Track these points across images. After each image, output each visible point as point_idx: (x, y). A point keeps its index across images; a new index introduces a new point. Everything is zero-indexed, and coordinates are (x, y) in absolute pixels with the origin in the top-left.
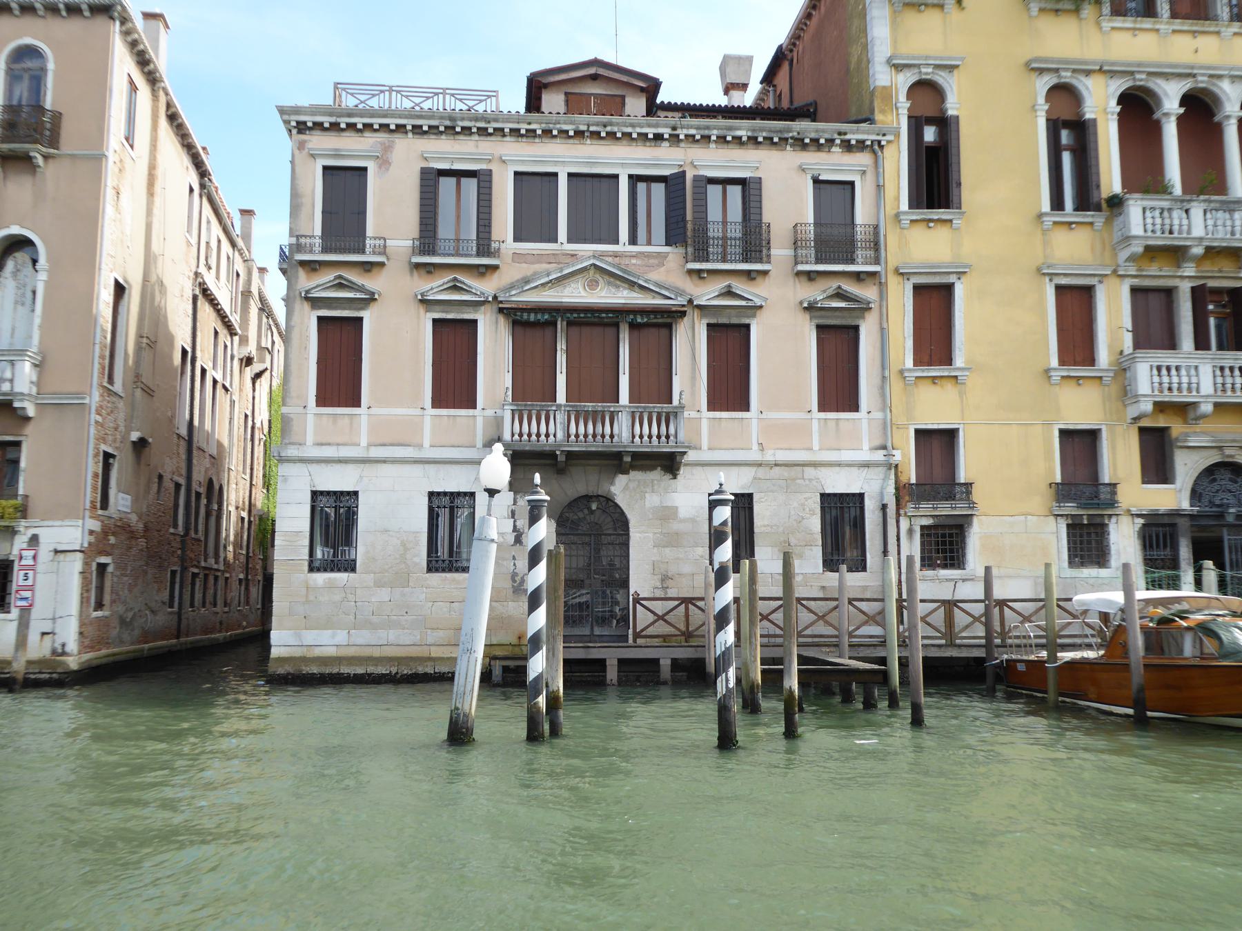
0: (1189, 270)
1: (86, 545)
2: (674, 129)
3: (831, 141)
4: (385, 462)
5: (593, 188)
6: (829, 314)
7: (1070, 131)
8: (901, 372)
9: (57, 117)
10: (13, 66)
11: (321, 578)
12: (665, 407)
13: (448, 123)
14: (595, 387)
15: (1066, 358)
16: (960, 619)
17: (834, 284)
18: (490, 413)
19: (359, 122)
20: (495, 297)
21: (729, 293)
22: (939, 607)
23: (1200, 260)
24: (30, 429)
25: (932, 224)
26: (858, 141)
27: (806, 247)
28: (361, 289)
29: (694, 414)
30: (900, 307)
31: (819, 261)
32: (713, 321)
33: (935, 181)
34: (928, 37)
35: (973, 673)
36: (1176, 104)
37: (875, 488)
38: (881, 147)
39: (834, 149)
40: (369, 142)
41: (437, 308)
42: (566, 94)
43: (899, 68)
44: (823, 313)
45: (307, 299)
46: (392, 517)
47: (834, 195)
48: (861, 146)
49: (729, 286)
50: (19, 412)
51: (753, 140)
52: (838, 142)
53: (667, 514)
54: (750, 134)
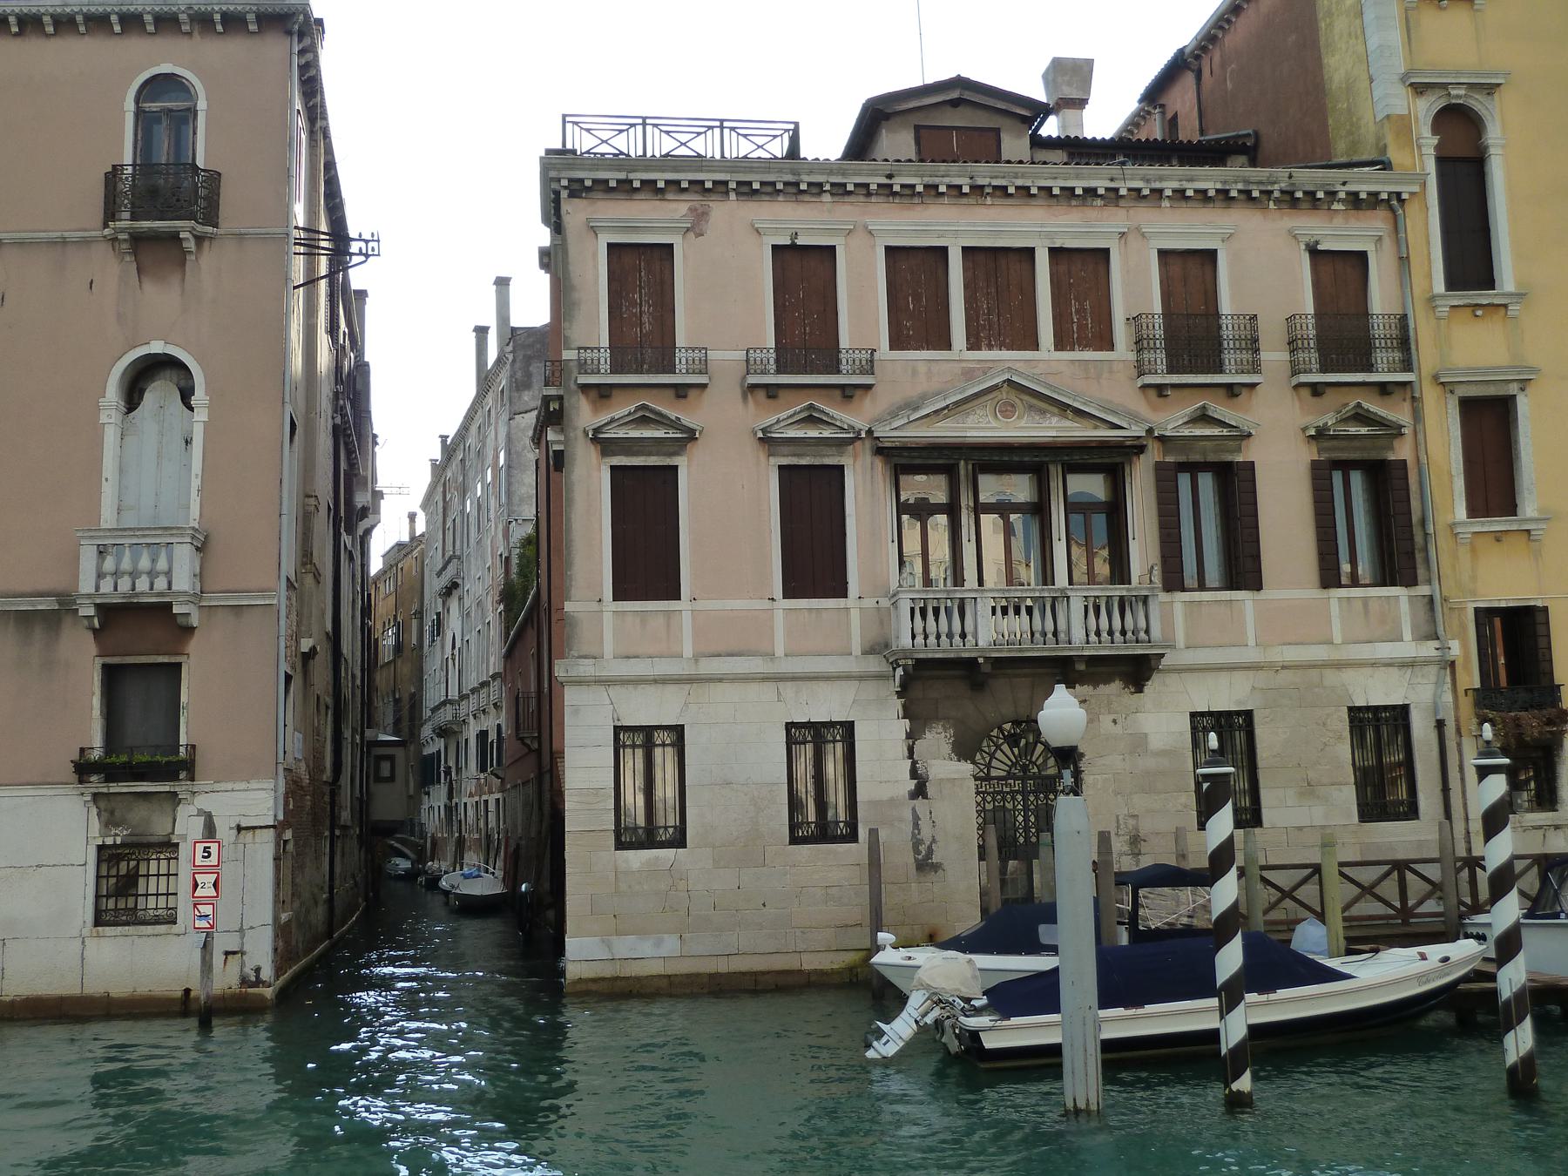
1: (281, 817)
2: (890, 176)
4: (721, 680)
5: (999, 268)
6: (1344, 444)
8: (1452, 526)
9: (214, 178)
10: (147, 106)
11: (637, 858)
13: (790, 178)
16: (1415, 885)
17: (1353, 400)
18: (869, 603)
19: (661, 178)
20: (870, 432)
21: (1203, 418)
22: (1387, 874)
24: (194, 645)
25: (1479, 313)
26: (1369, 194)
27: (1303, 349)
28: (675, 424)
31: (1324, 369)
32: (785, 461)
34: (1454, 47)
37: (1423, 697)
38: (1402, 201)
39: (1336, 206)
40: (678, 209)
41: (785, 449)
42: (917, 129)
43: (1420, 89)
44: (1335, 443)
45: (595, 440)
46: (738, 759)
47: (1341, 273)
48: (1374, 200)
49: (1204, 407)
50: (180, 620)
52: (1342, 195)
54: (1219, 186)
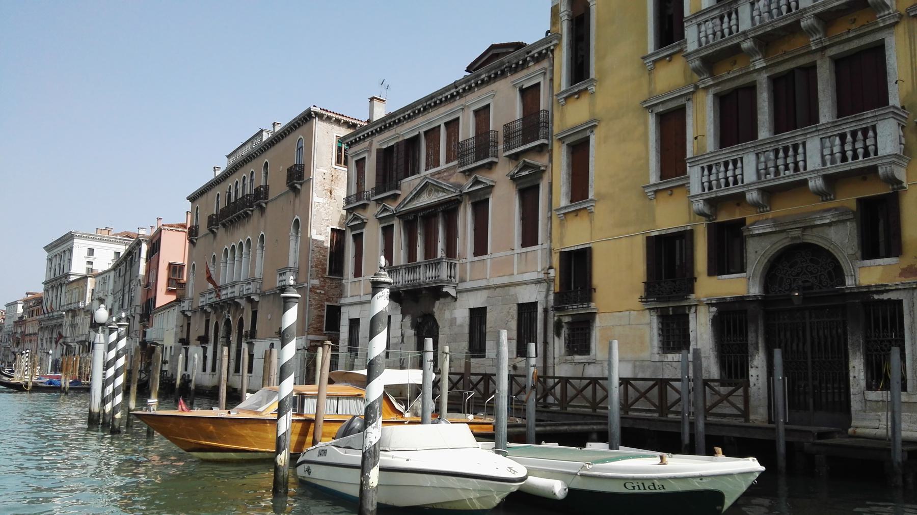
53: (453, 321)
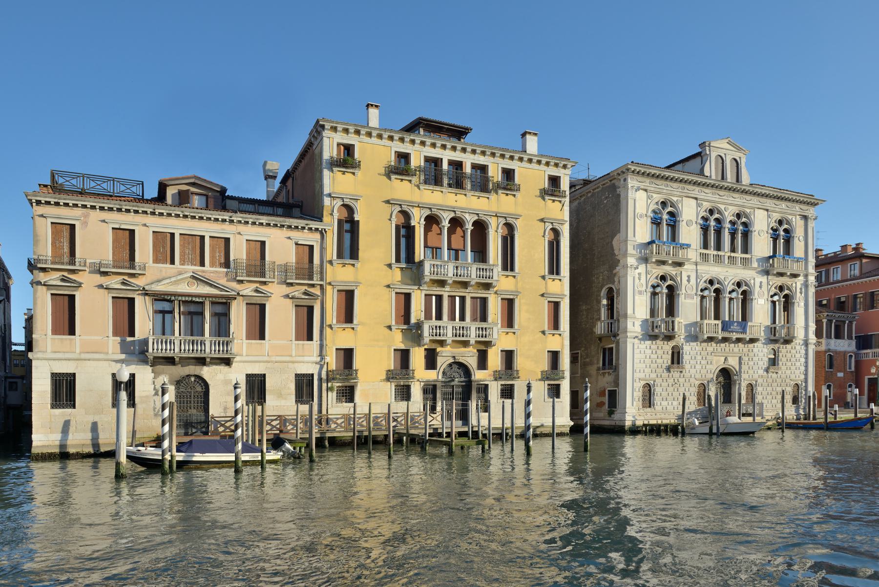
0: (447, 288)
3: (303, 228)
7: (405, 232)
12: (226, 339)
14: (194, 328)
15: (551, 272)
23: (451, 286)
28: (74, 281)
29: (240, 341)
30: (332, 301)
33: (350, 248)
35: (365, 443)
36: (447, 222)
51: (268, 225)
